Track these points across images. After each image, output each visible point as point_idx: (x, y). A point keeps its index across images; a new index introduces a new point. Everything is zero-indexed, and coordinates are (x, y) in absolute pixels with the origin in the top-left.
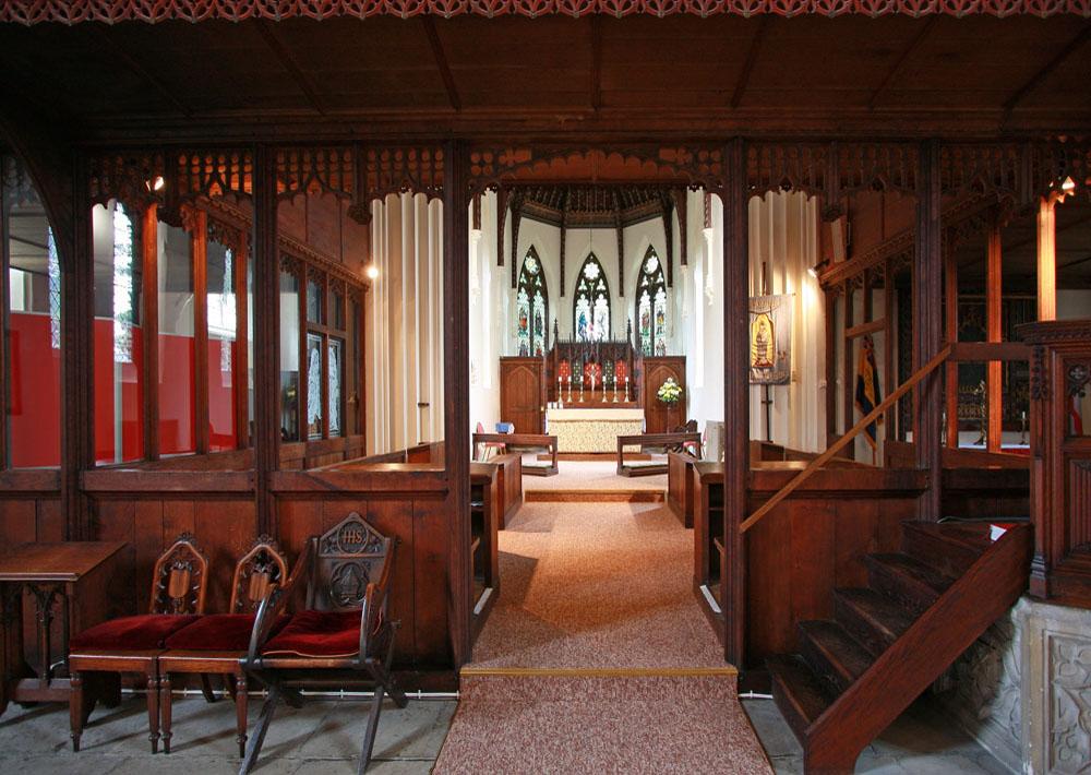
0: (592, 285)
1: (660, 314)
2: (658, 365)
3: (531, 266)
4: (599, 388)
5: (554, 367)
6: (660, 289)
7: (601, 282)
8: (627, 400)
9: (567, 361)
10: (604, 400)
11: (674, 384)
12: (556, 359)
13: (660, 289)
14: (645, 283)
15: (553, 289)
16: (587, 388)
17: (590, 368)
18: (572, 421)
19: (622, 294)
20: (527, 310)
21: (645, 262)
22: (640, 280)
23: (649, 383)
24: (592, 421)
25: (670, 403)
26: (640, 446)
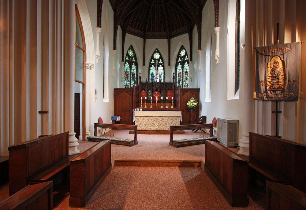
1: (186, 72)
2: (186, 92)
3: (131, 53)
4: (159, 102)
5: (139, 93)
6: (186, 63)
7: (161, 60)
8: (172, 107)
9: (145, 90)
10: (162, 107)
11: (194, 100)
12: (140, 89)
13: (186, 63)
14: (180, 60)
15: (140, 63)
16: (154, 101)
17: (156, 93)
19: (169, 65)
20: (128, 70)
23: (182, 99)
24: (156, 117)
25: (191, 109)
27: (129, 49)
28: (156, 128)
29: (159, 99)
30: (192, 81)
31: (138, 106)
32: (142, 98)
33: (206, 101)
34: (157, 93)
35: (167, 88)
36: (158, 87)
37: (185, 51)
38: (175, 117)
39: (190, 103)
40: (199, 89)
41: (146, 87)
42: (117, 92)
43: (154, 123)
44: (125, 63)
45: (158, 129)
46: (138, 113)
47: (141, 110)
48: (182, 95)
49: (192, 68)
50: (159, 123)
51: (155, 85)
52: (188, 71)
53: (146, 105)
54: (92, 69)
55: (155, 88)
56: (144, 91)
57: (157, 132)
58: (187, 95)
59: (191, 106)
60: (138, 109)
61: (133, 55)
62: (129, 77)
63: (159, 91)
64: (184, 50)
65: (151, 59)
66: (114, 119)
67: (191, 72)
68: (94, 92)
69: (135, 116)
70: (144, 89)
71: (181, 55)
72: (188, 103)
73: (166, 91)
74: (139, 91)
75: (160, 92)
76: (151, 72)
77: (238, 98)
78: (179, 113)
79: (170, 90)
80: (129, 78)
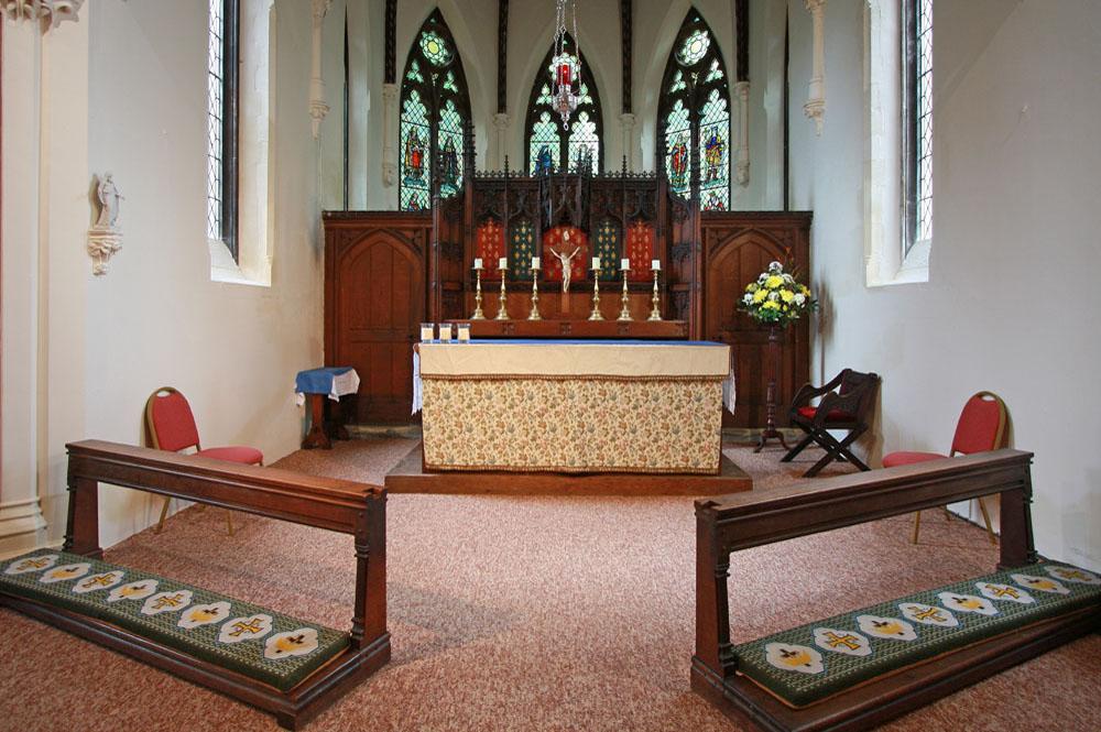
0: (695, 76)
1: (713, 144)
2: (734, 232)
3: (434, 49)
4: (581, 285)
5: (462, 235)
6: (715, 94)
8: (655, 316)
9: (498, 221)
10: (595, 316)
11: (787, 277)
12: (469, 214)
13: (715, 94)
14: (679, 85)
15: (482, 100)
16: (550, 284)
17: (559, 239)
18: (495, 379)
19: (627, 107)
20: (423, 134)
21: (679, 44)
22: (668, 80)
23: (711, 275)
24: (561, 379)
25: (769, 324)
26: (538, 267)
27: (426, 27)
28: (563, 458)
29: (578, 274)
30: (746, 182)
31: (454, 309)
32: (478, 264)
33: (872, 282)
34: (566, 236)
35: (625, 210)
36: (574, 205)
37: (710, 36)
38: (688, 380)
39: (765, 293)
40: (806, 219)
41: (506, 206)
42: (342, 229)
43: (551, 419)
44: (405, 95)
45: (578, 465)
46: (442, 354)
47: (464, 333)
48: (711, 251)
49: (745, 122)
50: (581, 425)
51: (558, 188)
52: (724, 135)
53: (506, 303)
54: (65, 26)
55: (556, 205)
56: (495, 226)
57: (568, 480)
58: (738, 249)
59: (770, 310)
60: (445, 331)
61: (445, 57)
62: (426, 165)
63: (578, 221)
64: (702, 31)
65: (536, 82)
66: (315, 386)
67: (744, 142)
68: (87, 208)
69: (424, 377)
70: (490, 214)
71: (687, 60)
72: (748, 297)
73: (616, 221)
74: (462, 224)
75: (585, 231)
76: (540, 146)
77: (925, 279)
78: (715, 359)
79: (645, 219)
80: (427, 172)
